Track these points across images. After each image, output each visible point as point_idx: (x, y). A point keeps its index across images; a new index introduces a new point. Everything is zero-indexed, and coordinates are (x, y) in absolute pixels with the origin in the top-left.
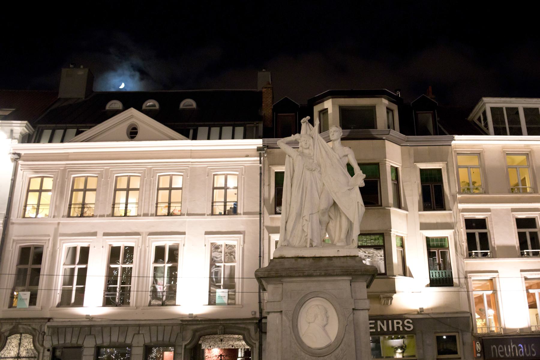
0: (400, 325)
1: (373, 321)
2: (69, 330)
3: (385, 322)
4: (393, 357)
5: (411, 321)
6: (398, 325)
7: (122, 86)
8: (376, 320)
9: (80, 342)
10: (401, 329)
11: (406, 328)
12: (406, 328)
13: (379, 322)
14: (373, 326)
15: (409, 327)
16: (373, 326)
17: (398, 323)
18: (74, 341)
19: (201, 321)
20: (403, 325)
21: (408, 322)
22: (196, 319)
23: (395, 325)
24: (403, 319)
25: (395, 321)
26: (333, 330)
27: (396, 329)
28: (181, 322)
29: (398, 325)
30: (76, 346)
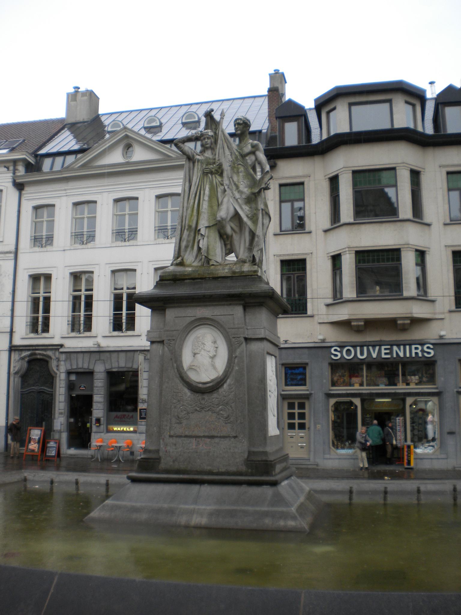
0: (418, 351)
1: (389, 347)
2: (304, 377)
3: (402, 347)
4: (392, 399)
5: (431, 346)
6: (416, 351)
7: (37, 487)
8: (392, 345)
9: (91, 367)
10: (420, 355)
11: (426, 354)
12: (426, 354)
13: (395, 348)
14: (388, 351)
15: (429, 353)
16: (388, 351)
17: (416, 348)
18: (86, 366)
19: (255, 306)
20: (423, 351)
21: (428, 348)
22: (79, 456)
23: (414, 351)
24: (422, 345)
25: (413, 347)
26: (221, 363)
27: (414, 355)
28: (198, 229)
29: (416, 351)
30: (87, 370)
